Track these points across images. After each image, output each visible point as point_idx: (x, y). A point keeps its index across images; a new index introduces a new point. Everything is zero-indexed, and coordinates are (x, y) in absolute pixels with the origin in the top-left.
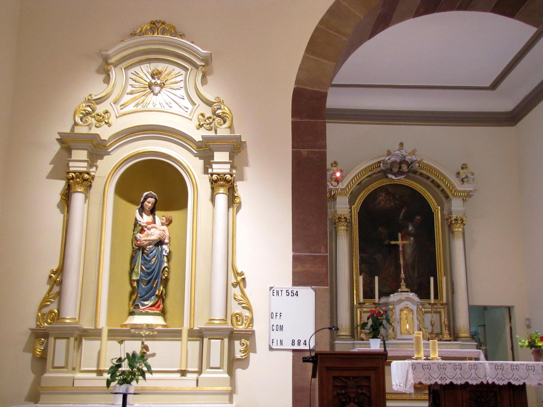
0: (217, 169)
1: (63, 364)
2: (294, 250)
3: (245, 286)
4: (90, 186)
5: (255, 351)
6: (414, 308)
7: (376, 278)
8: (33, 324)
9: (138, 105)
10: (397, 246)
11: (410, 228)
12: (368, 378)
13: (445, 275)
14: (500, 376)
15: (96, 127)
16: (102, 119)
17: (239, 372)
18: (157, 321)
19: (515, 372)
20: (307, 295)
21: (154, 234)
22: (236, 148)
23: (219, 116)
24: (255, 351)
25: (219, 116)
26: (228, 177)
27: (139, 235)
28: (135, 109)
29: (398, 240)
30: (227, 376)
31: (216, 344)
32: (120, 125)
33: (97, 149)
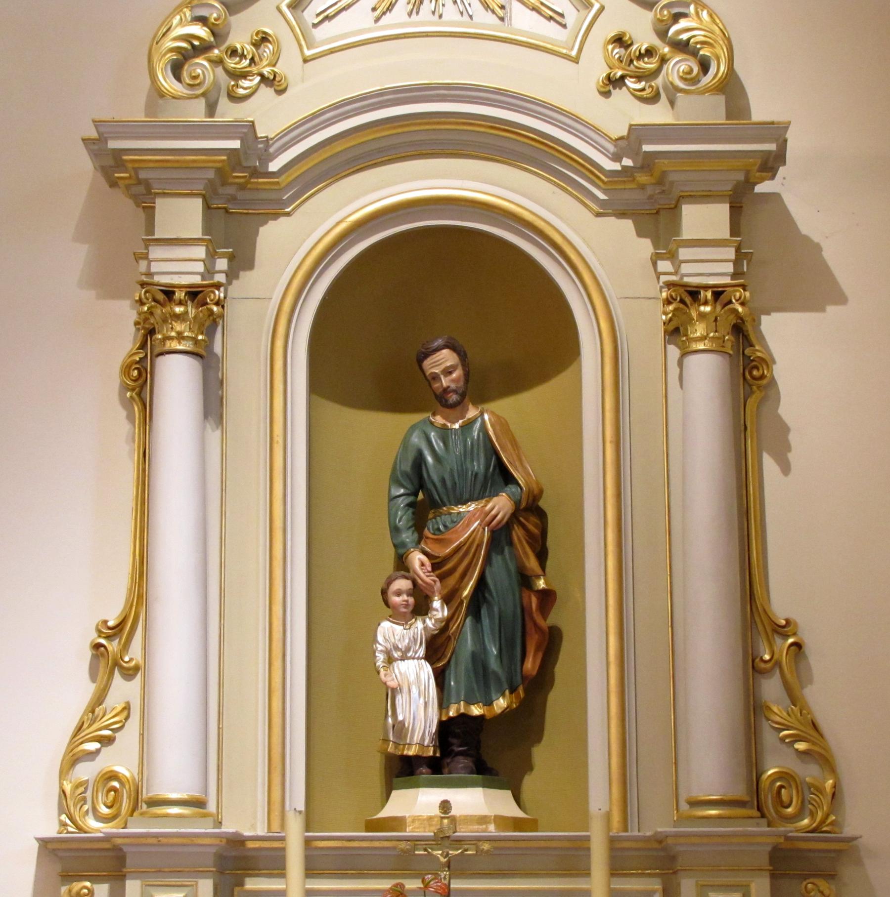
13: (495, 848)
15: (234, 98)
23: (682, 47)
29: (586, 873)
33: (241, 194)
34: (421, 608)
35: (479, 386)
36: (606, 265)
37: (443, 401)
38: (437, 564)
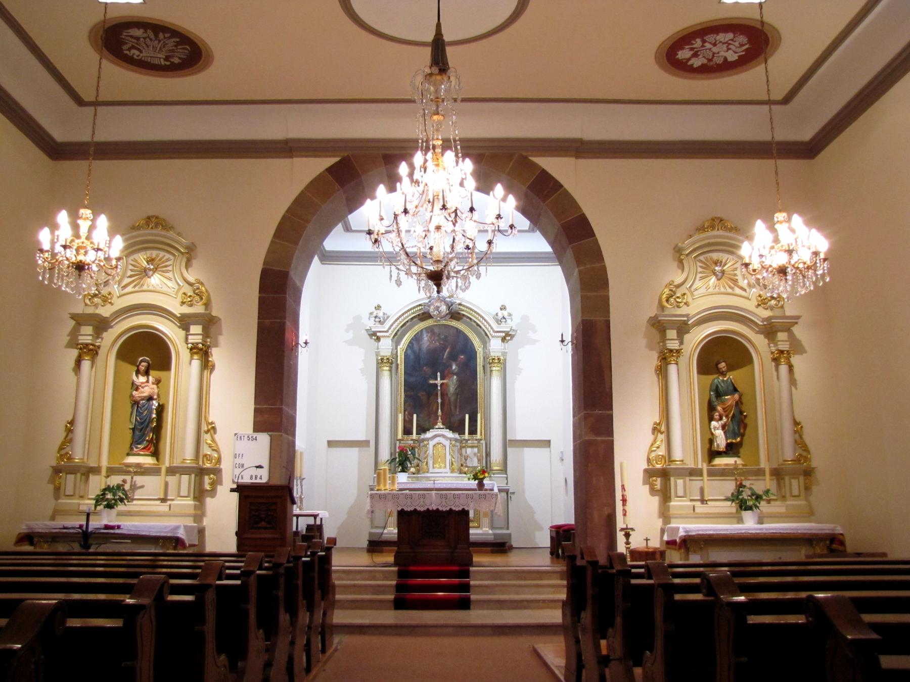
0: (192, 339)
1: (72, 493)
2: (256, 403)
3: (215, 433)
4: (97, 353)
5: (221, 484)
6: (447, 443)
7: (415, 416)
8: (54, 463)
9: (135, 286)
10: (436, 385)
11: (454, 367)
12: (276, 503)
14: (444, 503)
16: (106, 300)
17: (209, 501)
18: (147, 461)
19: (457, 500)
20: (264, 439)
21: (146, 391)
22: (209, 323)
24: (221, 484)
25: (197, 294)
26: (200, 345)
27: (134, 393)
28: (133, 290)
30: (190, 502)
31: (185, 478)
32: (120, 303)
33: (101, 325)
34: (721, 419)
35: (731, 368)
36: (759, 345)
37: (723, 374)
38: (724, 409)
